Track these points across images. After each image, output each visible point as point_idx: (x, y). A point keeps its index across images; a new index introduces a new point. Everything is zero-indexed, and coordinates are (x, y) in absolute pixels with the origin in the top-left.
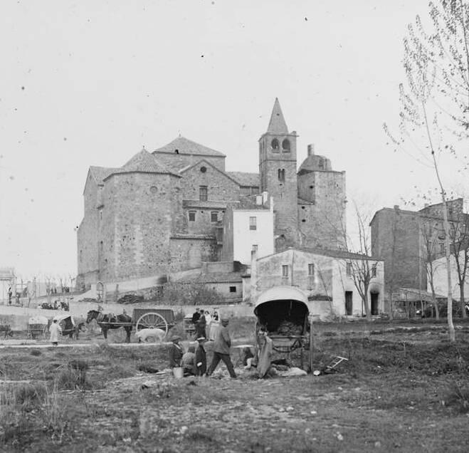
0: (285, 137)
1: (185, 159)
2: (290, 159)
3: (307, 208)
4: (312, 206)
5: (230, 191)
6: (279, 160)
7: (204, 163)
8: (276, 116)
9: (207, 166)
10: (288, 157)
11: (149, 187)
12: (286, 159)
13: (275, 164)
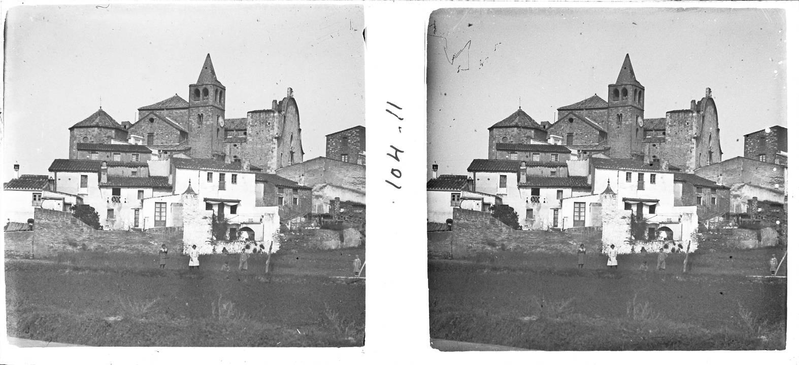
0: (623, 86)
1: (160, 113)
2: (627, 105)
3: (657, 145)
4: (663, 144)
5: (591, 135)
6: (198, 107)
7: (571, 115)
8: (204, 69)
9: (155, 117)
10: (207, 103)
11: (82, 138)
12: (624, 105)
13: (615, 110)
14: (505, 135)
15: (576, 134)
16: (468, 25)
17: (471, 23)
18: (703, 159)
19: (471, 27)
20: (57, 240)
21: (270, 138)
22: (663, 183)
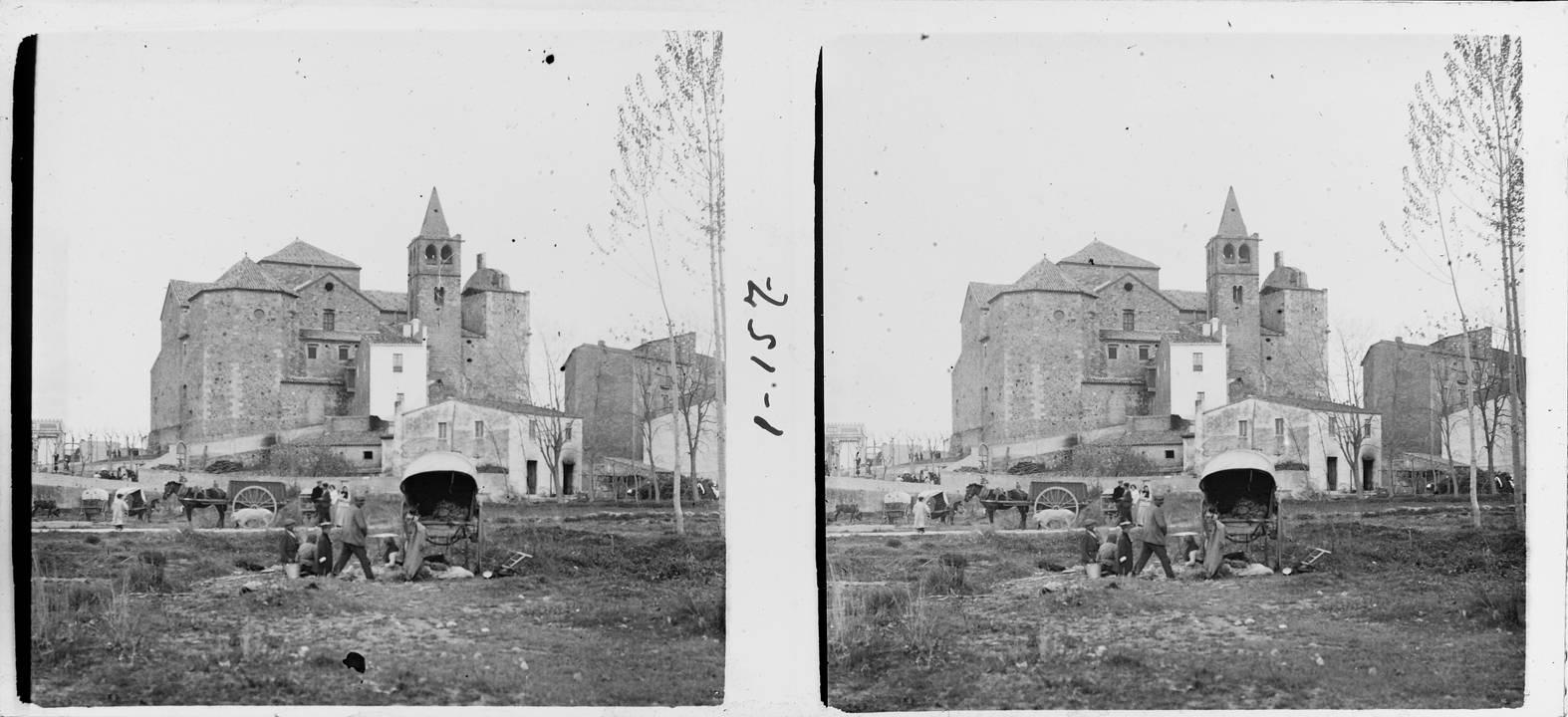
5: (1165, 316)
6: (1234, 274)
12: (1245, 272)
14: (260, 305)
15: (1140, 313)
16: (920, 36)
17: (926, 34)
18: (595, 638)
19: (926, 40)
20: (1399, 579)
21: (521, 334)
22: (1479, 235)
